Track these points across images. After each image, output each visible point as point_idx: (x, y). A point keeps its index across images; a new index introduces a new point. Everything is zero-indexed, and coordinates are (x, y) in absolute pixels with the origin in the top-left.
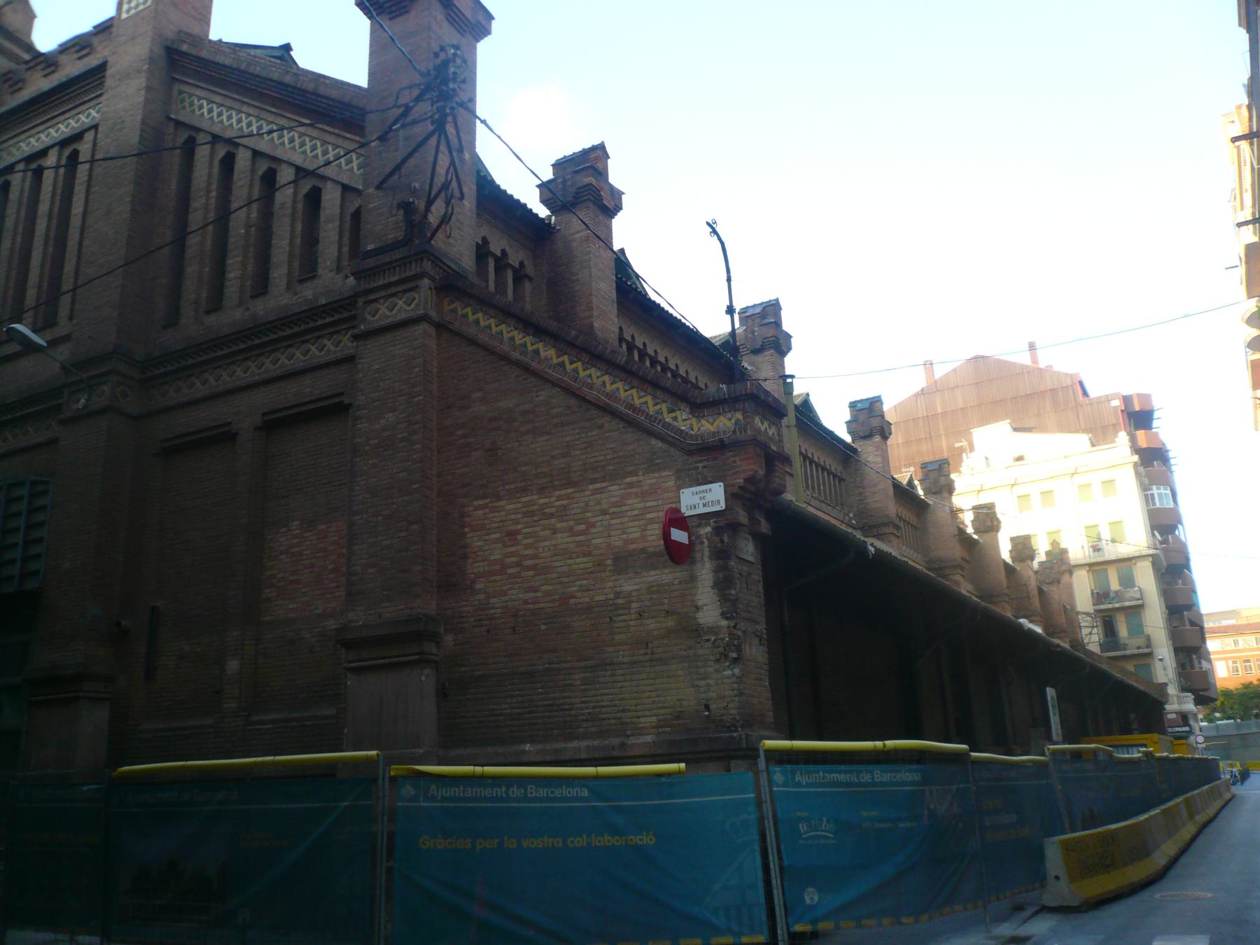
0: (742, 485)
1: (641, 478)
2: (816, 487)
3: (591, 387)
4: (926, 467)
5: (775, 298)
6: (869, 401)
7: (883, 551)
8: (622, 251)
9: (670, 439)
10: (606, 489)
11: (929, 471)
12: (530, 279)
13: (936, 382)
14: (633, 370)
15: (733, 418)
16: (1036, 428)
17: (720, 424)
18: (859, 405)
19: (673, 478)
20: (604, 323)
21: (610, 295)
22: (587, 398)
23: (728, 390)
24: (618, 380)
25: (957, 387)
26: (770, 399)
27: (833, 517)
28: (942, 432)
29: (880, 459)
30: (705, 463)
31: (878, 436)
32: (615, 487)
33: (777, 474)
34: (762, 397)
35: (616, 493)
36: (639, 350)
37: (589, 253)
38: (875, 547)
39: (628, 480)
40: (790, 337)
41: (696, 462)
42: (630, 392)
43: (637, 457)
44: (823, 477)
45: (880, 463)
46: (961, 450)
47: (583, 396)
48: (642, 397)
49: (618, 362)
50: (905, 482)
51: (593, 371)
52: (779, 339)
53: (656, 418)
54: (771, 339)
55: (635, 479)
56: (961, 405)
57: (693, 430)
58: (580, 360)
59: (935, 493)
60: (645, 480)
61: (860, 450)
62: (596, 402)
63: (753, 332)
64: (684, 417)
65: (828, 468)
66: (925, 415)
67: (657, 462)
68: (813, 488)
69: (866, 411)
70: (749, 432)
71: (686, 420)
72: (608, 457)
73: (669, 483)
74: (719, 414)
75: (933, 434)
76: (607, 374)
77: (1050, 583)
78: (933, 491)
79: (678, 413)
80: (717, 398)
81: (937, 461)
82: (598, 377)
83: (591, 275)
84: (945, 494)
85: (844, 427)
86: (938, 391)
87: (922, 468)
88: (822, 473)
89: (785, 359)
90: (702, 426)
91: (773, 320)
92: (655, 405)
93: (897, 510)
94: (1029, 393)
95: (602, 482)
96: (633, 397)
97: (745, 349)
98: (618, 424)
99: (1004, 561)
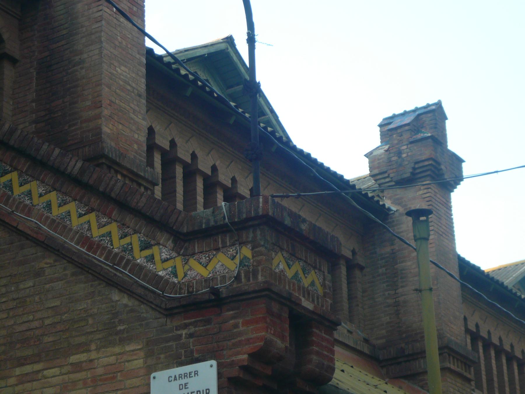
0: (246, 363)
1: (93, 355)
3: (29, 210)
5: (435, 101)
9: (140, 291)
10: (40, 375)
12: (13, 61)
14: (91, 182)
15: (238, 256)
17: (218, 266)
19: (142, 354)
20: (120, 126)
21: (134, 85)
22: (20, 227)
23: (229, 211)
24: (68, 199)
26: (304, 227)
30: (192, 330)
32: (56, 371)
33: (315, 348)
34: (288, 221)
35: (54, 380)
36: (206, 178)
37: (99, 20)
39: (74, 359)
41: (178, 328)
42: (85, 218)
43: (90, 321)
47: (15, 225)
48: (104, 226)
49: (69, 169)
51: (35, 187)
52: (439, 164)
53: (122, 258)
54: (427, 163)
55: (82, 357)
57: (176, 276)
58: (15, 169)
60: (98, 359)
62: (35, 236)
63: (399, 153)
64: (164, 256)
67: (119, 328)
70: (260, 278)
71: (166, 260)
72: (47, 322)
73: (136, 362)
74: (217, 250)
76: (55, 189)
79: (155, 250)
80: (212, 223)
82: (41, 196)
83: (101, 53)
89: (452, 194)
90: (191, 269)
91: (429, 135)
92: (121, 238)
95: (35, 362)
96: (90, 225)
97: (387, 180)
98: (65, 269)
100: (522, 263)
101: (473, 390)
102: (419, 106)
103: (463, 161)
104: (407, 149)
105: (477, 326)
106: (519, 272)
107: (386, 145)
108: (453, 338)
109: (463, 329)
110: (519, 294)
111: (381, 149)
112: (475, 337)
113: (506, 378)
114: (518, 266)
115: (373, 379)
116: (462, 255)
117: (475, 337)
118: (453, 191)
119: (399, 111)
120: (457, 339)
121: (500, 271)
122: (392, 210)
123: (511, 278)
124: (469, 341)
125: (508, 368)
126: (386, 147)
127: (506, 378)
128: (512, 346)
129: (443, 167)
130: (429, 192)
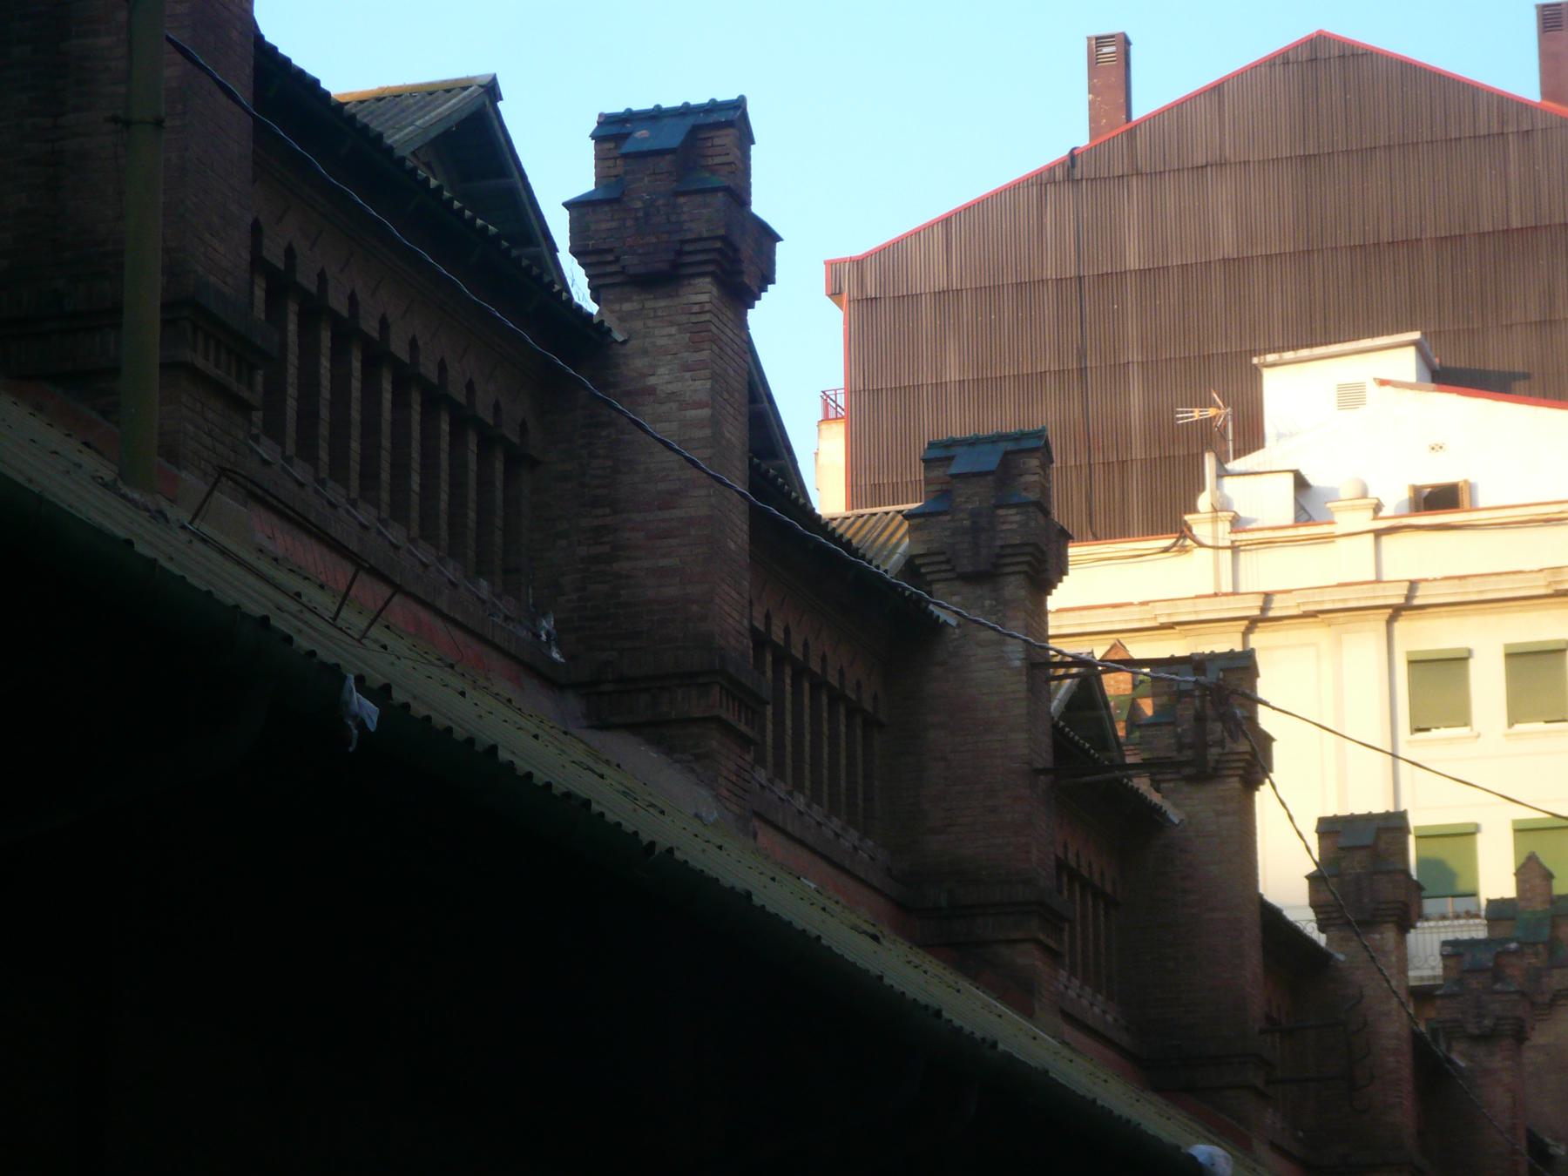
2: (385, 476)
6: (690, 121)
13: (1131, 133)
16: (1526, 376)
18: (642, 133)
25: (1222, 164)
27: (447, 618)
28: (1134, 355)
31: (705, 283)
44: (429, 434)
45: (699, 405)
46: (1206, 436)
56: (1227, 244)
59: (974, 578)
65: (460, 396)
68: (369, 477)
69: (664, 163)
77: (1486, 1038)
78: (966, 566)
84: (1014, 588)
87: (928, 462)
88: (400, 403)
94: (1515, 223)
99: (1271, 917)
101: (256, 439)
103: (779, 239)
105: (290, 253)
106: (433, 114)
108: (212, 279)
109: (246, 255)
110: (422, 173)
112: (280, 284)
113: (355, 415)
114: (436, 94)
115: (275, 563)
116: (270, 36)
117: (280, 284)
120: (225, 283)
121: (381, 103)
123: (411, 128)
124: (259, 293)
125: (812, 698)
127: (355, 415)
128: (384, 324)
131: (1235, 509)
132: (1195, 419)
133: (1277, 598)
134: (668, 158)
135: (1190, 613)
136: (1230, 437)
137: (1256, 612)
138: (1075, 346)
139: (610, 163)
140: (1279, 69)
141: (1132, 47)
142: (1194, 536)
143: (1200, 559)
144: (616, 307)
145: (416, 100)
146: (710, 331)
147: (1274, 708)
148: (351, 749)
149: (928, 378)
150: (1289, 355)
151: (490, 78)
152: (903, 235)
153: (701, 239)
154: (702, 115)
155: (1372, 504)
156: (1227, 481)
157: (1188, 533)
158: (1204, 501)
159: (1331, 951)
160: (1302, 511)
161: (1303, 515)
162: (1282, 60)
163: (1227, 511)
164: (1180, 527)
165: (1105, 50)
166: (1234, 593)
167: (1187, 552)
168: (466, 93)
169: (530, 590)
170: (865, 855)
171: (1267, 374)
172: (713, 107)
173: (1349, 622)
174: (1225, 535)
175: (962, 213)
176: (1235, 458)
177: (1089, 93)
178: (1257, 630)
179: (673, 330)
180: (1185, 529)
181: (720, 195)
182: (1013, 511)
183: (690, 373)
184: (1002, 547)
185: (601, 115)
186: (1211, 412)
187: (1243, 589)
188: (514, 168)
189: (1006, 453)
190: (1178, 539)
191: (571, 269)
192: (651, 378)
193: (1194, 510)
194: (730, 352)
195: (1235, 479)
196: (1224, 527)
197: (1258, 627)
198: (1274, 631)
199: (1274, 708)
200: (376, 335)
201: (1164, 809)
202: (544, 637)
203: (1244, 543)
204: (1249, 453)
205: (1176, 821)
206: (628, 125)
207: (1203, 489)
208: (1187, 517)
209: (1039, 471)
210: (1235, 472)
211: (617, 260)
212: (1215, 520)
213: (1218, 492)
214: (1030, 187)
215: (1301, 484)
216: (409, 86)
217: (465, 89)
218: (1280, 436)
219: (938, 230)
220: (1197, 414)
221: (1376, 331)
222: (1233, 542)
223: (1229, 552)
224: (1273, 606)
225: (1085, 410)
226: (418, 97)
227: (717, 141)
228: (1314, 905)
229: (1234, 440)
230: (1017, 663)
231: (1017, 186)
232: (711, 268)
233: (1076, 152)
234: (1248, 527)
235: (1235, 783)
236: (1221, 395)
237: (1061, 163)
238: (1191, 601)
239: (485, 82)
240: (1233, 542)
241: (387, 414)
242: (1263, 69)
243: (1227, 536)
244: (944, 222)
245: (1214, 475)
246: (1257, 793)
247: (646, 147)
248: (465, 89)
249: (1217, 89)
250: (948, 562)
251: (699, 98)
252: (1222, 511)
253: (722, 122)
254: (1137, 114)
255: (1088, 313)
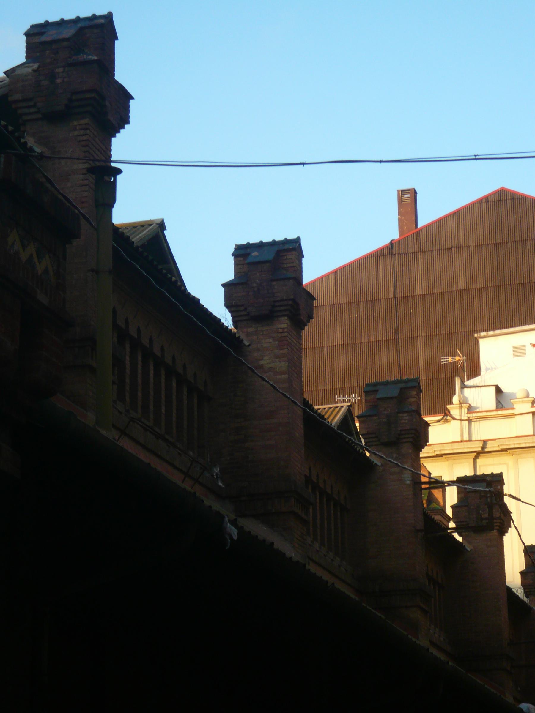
4: (376, 391)
5: (105, 12)
6: (276, 248)
7: (249, 532)
8: (5, 73)
11: (378, 399)
13: (418, 233)
18: (255, 254)
25: (459, 247)
28: (421, 333)
29: (283, 365)
31: (284, 319)
38: (240, 529)
40: (129, 97)
45: (283, 373)
50: (335, 420)
54: (87, 95)
56: (462, 284)
59: (388, 444)
61: (246, 343)
66: (392, 296)
75: (401, 336)
81: (396, 382)
84: (406, 449)
85: (220, 293)
86: (422, 251)
87: (366, 392)
93: (310, 469)
97: (32, 110)
99: (509, 590)
100: (141, 225)
102: (82, 16)
103: (132, 98)
104: (62, 72)
106: (138, 237)
107: (34, 63)
111: (28, 67)
113: (140, 380)
114: (137, 227)
118: (115, 136)
119: (54, 18)
122: (35, 152)
126: (35, 66)
127: (140, 380)
129: (107, 103)
130: (87, 134)
131: (469, 403)
132: (450, 362)
133: (489, 443)
134: (268, 264)
135: (450, 450)
136: (465, 370)
137: (480, 449)
138: (393, 329)
139: (240, 267)
140: (484, 205)
141: (417, 195)
142: (451, 415)
143: (454, 425)
144: (245, 330)
145: (128, 230)
146: (287, 340)
147: (523, 502)
148: (227, 548)
149: (328, 344)
150: (491, 333)
151: (161, 220)
152: (317, 278)
153: (282, 300)
154: (281, 245)
155: (531, 400)
156: (466, 390)
157: (448, 413)
158: (455, 399)
159: (531, 606)
160: (499, 403)
161: (500, 405)
162: (485, 201)
163: (466, 404)
164: (445, 411)
165: (405, 196)
166: (470, 441)
167: (448, 422)
168: (151, 227)
169: (209, 455)
170: (343, 569)
171: (481, 341)
172: (286, 241)
173: (520, 454)
174: (465, 416)
175: (342, 269)
176: (467, 381)
177: (399, 215)
178: (480, 457)
179: (271, 340)
180: (447, 412)
181: (291, 281)
182: (405, 415)
183: (278, 359)
184: (401, 431)
185: (236, 245)
186: (457, 358)
187: (473, 439)
188: (171, 259)
189: (401, 389)
190: (444, 416)
191: (225, 314)
192: (261, 361)
193: (451, 403)
194: (295, 350)
195: (469, 389)
196: (465, 411)
197: (480, 456)
198: (488, 458)
199: (523, 502)
200: (148, 345)
201: (29, 145)
202: (215, 476)
203: (473, 418)
204: (475, 377)
205: (469, 550)
206: (248, 250)
207: (455, 394)
208: (448, 406)
209: (416, 396)
210: (468, 386)
211: (246, 309)
212: (460, 408)
213: (461, 395)
214: (373, 258)
215: (499, 391)
216: (124, 224)
217: (151, 225)
218: (487, 369)
219: (332, 277)
220: (450, 359)
221: (529, 323)
222: (469, 417)
223: (467, 422)
224: (487, 446)
225: (398, 356)
226: (129, 229)
227: (288, 257)
228: (523, 585)
229: (466, 371)
230: (408, 482)
231: (367, 257)
232: (287, 313)
233: (393, 242)
234: (475, 411)
235: (495, 532)
236: (462, 352)
237: (386, 246)
238: (450, 444)
239: (159, 222)
240: (469, 417)
241: (152, 380)
242: (477, 204)
243: (466, 415)
244: (334, 273)
245: (460, 387)
246: (504, 537)
247: (257, 260)
248: (151, 225)
249: (456, 213)
250: (377, 437)
251: (279, 238)
252: (463, 404)
253: (291, 249)
254: (421, 223)
255: (399, 313)
